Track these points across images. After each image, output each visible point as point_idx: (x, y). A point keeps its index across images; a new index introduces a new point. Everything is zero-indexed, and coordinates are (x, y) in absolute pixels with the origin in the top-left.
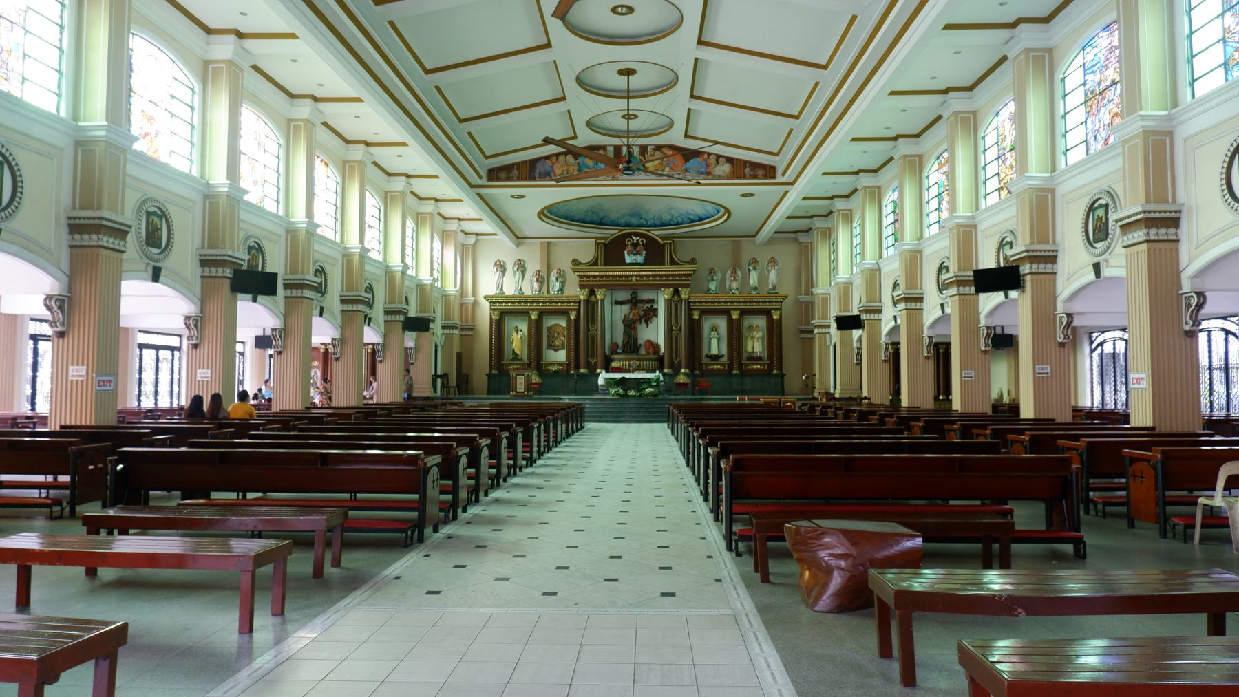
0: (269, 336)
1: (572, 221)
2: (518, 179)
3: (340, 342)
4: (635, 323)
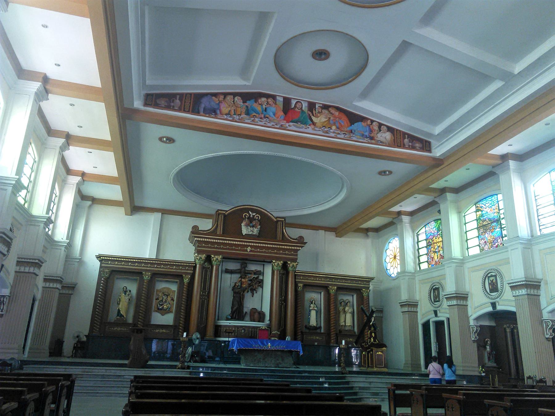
2: (179, 110)
4: (244, 292)
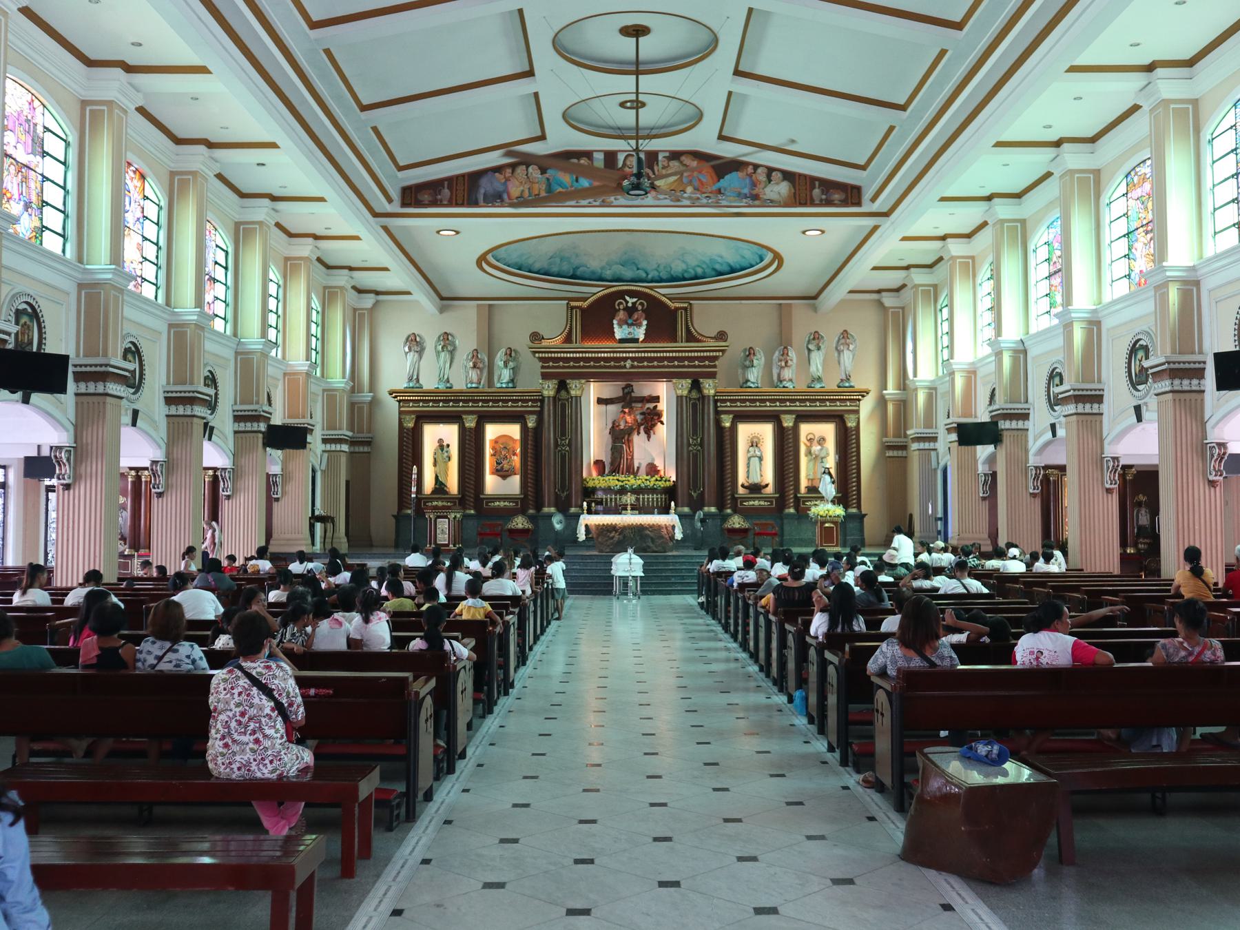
0: (49, 458)
1: (530, 272)
2: (450, 205)
3: (169, 465)
